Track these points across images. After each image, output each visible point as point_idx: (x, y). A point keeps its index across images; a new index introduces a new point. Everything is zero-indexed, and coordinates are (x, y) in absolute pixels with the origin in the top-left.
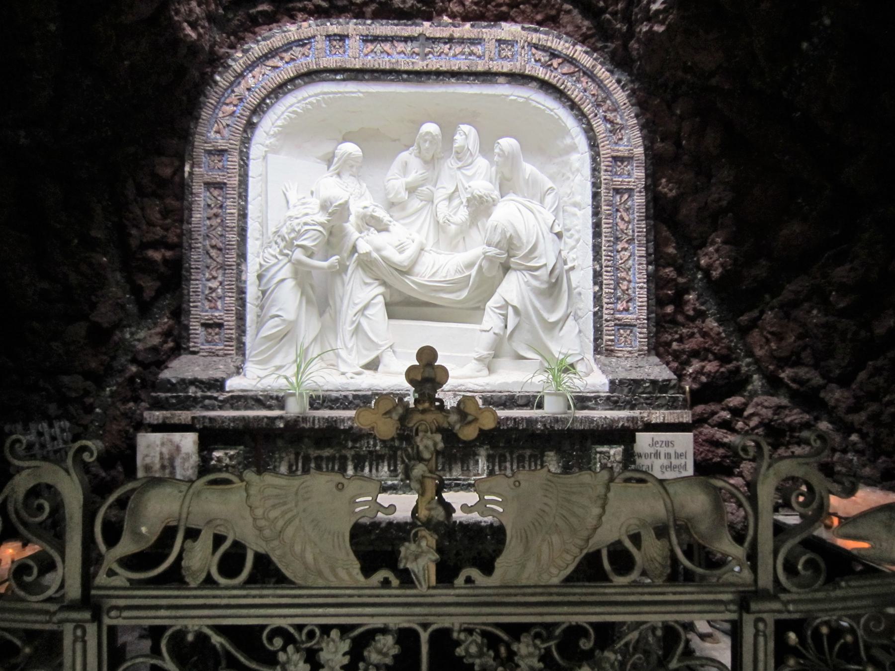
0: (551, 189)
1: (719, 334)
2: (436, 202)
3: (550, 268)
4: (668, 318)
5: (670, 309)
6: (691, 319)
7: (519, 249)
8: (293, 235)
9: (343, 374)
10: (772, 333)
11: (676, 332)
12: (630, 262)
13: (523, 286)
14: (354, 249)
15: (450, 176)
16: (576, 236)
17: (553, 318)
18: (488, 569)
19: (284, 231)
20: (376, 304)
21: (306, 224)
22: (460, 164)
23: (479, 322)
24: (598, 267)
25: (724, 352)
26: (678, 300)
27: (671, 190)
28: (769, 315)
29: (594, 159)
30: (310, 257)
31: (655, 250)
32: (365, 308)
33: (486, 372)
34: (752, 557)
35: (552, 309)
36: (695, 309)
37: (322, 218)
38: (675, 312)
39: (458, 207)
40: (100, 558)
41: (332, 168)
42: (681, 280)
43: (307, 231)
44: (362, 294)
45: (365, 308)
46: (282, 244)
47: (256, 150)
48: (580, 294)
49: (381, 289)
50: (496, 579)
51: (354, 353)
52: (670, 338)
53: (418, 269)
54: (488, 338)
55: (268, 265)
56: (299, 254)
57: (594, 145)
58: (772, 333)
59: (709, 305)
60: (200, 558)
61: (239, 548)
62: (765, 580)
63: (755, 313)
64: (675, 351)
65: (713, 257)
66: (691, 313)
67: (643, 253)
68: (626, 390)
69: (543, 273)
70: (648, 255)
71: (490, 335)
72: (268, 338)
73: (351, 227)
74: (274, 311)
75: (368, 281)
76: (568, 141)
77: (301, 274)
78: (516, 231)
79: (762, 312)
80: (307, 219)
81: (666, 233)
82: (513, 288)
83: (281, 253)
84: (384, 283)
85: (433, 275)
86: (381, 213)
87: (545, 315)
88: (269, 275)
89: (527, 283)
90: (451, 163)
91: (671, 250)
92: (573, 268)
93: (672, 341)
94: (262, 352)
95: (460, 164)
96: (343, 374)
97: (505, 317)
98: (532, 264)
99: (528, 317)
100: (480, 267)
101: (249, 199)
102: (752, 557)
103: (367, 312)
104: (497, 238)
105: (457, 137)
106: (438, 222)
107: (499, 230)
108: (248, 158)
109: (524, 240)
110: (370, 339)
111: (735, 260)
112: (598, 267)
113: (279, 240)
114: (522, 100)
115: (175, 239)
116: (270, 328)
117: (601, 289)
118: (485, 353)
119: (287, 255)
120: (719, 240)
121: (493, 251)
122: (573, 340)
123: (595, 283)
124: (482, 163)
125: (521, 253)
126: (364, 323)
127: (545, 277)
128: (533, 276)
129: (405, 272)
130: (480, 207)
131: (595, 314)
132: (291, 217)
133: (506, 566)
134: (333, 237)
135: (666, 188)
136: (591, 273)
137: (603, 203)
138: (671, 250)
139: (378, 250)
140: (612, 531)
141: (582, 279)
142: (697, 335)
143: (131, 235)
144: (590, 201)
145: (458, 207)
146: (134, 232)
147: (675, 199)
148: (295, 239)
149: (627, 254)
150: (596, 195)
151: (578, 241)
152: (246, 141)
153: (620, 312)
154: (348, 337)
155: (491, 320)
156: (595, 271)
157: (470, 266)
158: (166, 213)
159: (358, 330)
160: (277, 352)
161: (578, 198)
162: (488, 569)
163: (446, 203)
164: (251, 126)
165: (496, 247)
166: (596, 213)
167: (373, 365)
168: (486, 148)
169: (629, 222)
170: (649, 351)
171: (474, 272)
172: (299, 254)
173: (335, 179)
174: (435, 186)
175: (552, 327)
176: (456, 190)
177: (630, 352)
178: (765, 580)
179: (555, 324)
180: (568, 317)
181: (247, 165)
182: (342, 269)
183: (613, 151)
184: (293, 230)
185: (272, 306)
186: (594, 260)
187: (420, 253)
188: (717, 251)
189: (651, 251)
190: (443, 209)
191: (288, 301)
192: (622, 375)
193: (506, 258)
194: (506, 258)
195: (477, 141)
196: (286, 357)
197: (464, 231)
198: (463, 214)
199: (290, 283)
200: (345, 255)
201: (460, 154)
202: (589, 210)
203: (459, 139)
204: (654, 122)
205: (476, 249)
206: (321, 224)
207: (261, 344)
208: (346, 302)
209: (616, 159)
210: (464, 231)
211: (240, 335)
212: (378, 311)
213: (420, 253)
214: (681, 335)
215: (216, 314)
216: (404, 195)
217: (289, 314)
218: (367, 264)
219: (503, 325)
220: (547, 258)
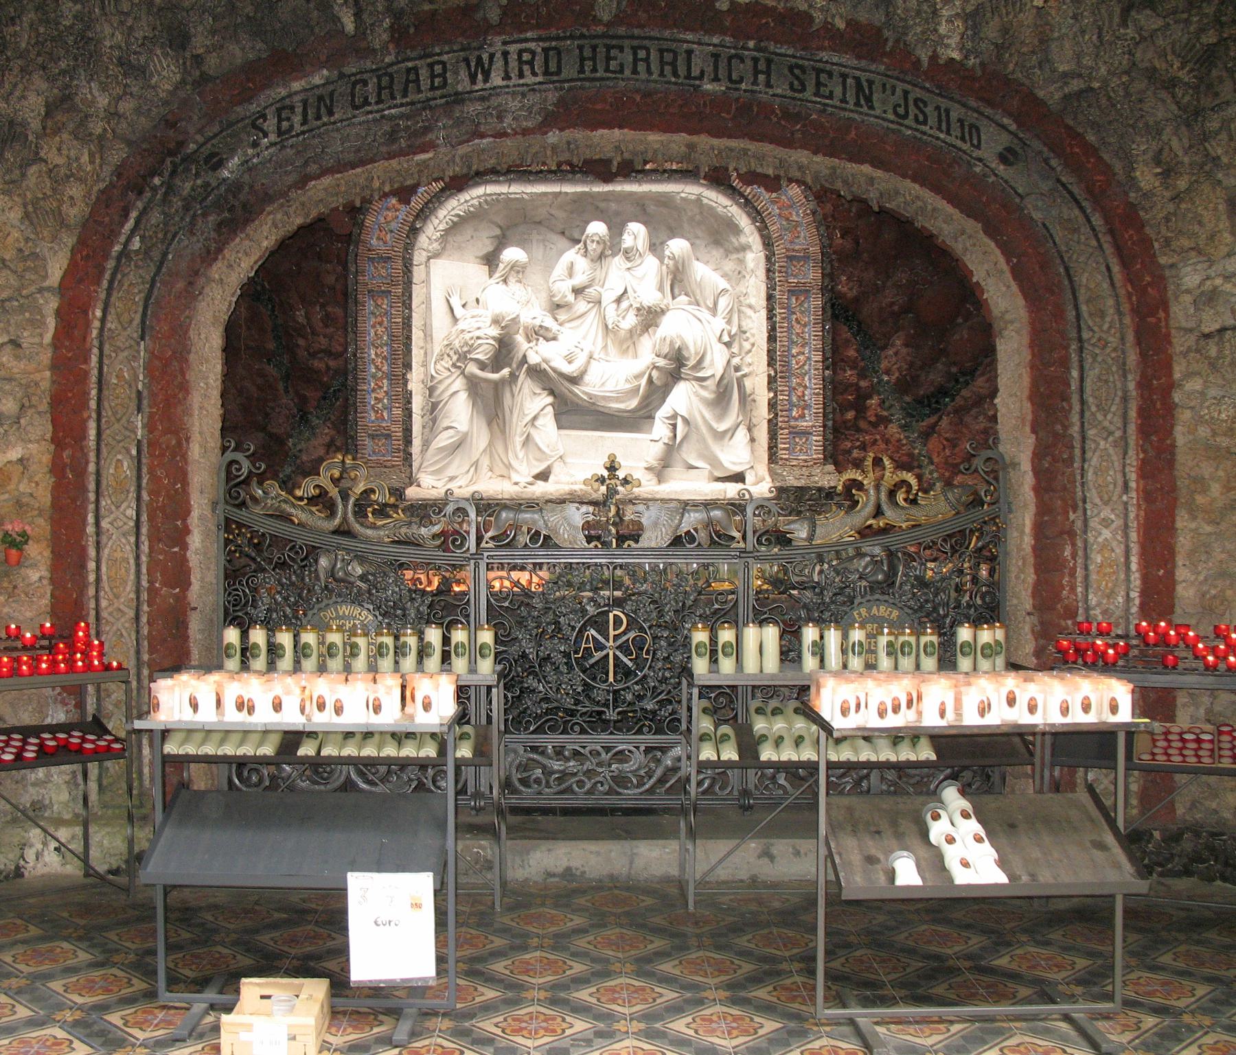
0: (724, 291)
1: (899, 440)
2: (603, 305)
3: (718, 378)
4: (849, 424)
5: (850, 415)
6: (874, 425)
7: (687, 359)
8: (465, 349)
9: (516, 484)
10: (947, 439)
11: (858, 440)
12: (806, 367)
13: (693, 398)
14: (524, 359)
15: (616, 274)
16: (752, 340)
17: (722, 427)
18: (637, 541)
19: (457, 344)
20: (545, 415)
21: (478, 338)
22: (629, 265)
23: (649, 431)
24: (772, 373)
25: (905, 459)
26: (859, 406)
27: (851, 289)
28: (945, 422)
29: (768, 259)
30: (482, 369)
31: (833, 353)
32: (535, 418)
33: (655, 480)
34: (744, 538)
35: (721, 417)
36: (876, 415)
37: (495, 332)
38: (856, 418)
39: (627, 310)
40: (482, 537)
41: (497, 275)
42: (863, 384)
43: (480, 345)
44: (532, 403)
45: (535, 418)
46: (455, 358)
47: (419, 257)
48: (754, 401)
49: (550, 399)
50: (640, 545)
51: (525, 463)
52: (849, 445)
53: (587, 378)
54: (658, 449)
55: (440, 378)
56: (472, 369)
57: (768, 243)
58: (947, 439)
59: (893, 411)
60: (524, 539)
61: (538, 533)
62: (750, 548)
63: (933, 420)
64: (855, 459)
65: (894, 359)
66: (873, 419)
67: (819, 358)
68: (792, 498)
69: (711, 383)
70: (825, 359)
71: (660, 444)
72: (441, 449)
73: (520, 338)
74: (446, 423)
75: (538, 391)
76: (743, 240)
77: (473, 385)
78: (684, 343)
79: (940, 418)
80: (478, 333)
81: (846, 333)
82: (683, 398)
83: (454, 365)
84: (552, 392)
85: (603, 384)
86: (549, 322)
87: (715, 425)
88: (441, 388)
89: (695, 393)
90: (618, 260)
91: (852, 353)
92: (745, 376)
93: (853, 447)
94: (436, 462)
95: (629, 265)
96: (516, 484)
97: (674, 426)
98: (700, 375)
99: (697, 428)
100: (650, 377)
101: (414, 306)
102: (744, 538)
103: (537, 423)
104: (666, 350)
105: (625, 236)
106: (607, 326)
107: (668, 342)
108: (411, 265)
109: (692, 350)
110: (539, 449)
111: (911, 365)
112: (772, 373)
113: (452, 353)
114: (693, 197)
115: (340, 349)
116: (443, 440)
117: (776, 395)
118: (655, 463)
119: (459, 367)
120: (898, 343)
121: (662, 362)
122: (742, 452)
123: (770, 389)
124: (651, 262)
125: (691, 363)
126: (533, 432)
127: (714, 388)
128: (702, 387)
129: (575, 380)
130: (650, 318)
131: (769, 421)
132: (463, 331)
133: (644, 542)
134: (504, 350)
135: (844, 287)
136: (766, 379)
137: (777, 307)
138: (852, 353)
139: (544, 361)
140: (685, 527)
141: (758, 385)
142: (880, 442)
143: (298, 345)
144: (764, 303)
145: (627, 310)
146: (301, 342)
147: (856, 300)
148: (469, 352)
149: (801, 357)
150: (770, 298)
151: (753, 345)
152: (409, 247)
153: (796, 419)
154: (518, 447)
155: (660, 429)
156: (769, 376)
157: (638, 377)
158: (328, 320)
159: (528, 440)
160: (448, 464)
161: (752, 301)
162: (637, 541)
163: (614, 306)
164: (414, 232)
165: (665, 357)
166: (770, 317)
167: (543, 476)
168: (656, 247)
169: (805, 325)
170: (825, 458)
171: (644, 381)
172: (472, 369)
173: (502, 286)
174: (603, 286)
175: (720, 436)
176: (626, 291)
177: (806, 461)
178: (750, 548)
179: (725, 432)
180: (738, 426)
181: (410, 272)
182: (513, 377)
183: (788, 250)
184: (466, 344)
185: (446, 417)
186: (769, 365)
187: (589, 362)
188: (896, 354)
189: (829, 355)
190: (611, 312)
191: (460, 412)
192: (792, 481)
193: (677, 366)
194: (677, 366)
195: (647, 240)
196: (458, 466)
197: (633, 335)
198: (630, 321)
199: (463, 396)
200: (514, 366)
201: (628, 254)
202: (764, 313)
203: (627, 241)
204: (833, 216)
205: (646, 356)
206: (494, 338)
207: (435, 455)
208: (515, 416)
209: (790, 258)
210: (633, 335)
211: (406, 446)
212: (548, 421)
213: (589, 362)
214: (863, 443)
215: (384, 425)
216: (571, 298)
217: (463, 426)
218: (538, 373)
219: (671, 435)
220: (717, 362)
